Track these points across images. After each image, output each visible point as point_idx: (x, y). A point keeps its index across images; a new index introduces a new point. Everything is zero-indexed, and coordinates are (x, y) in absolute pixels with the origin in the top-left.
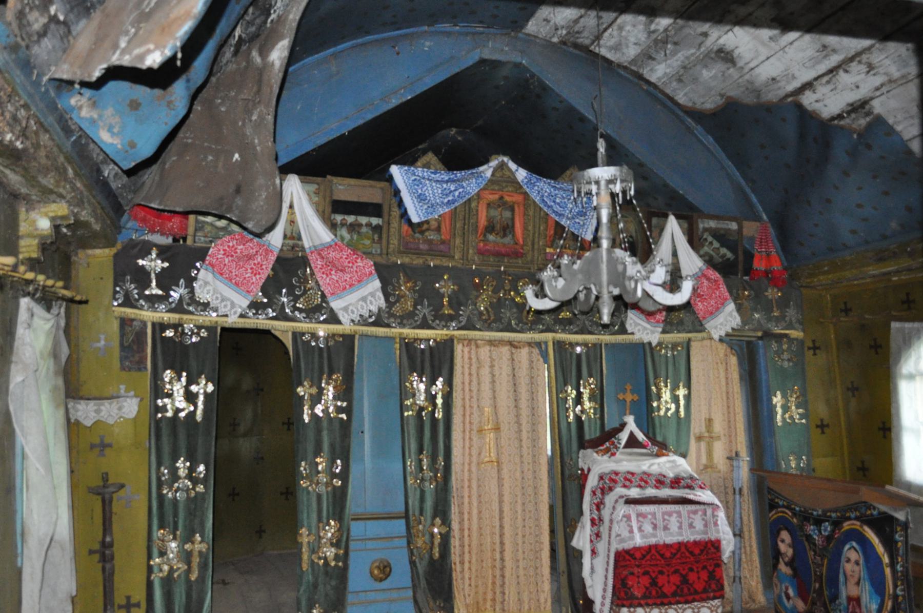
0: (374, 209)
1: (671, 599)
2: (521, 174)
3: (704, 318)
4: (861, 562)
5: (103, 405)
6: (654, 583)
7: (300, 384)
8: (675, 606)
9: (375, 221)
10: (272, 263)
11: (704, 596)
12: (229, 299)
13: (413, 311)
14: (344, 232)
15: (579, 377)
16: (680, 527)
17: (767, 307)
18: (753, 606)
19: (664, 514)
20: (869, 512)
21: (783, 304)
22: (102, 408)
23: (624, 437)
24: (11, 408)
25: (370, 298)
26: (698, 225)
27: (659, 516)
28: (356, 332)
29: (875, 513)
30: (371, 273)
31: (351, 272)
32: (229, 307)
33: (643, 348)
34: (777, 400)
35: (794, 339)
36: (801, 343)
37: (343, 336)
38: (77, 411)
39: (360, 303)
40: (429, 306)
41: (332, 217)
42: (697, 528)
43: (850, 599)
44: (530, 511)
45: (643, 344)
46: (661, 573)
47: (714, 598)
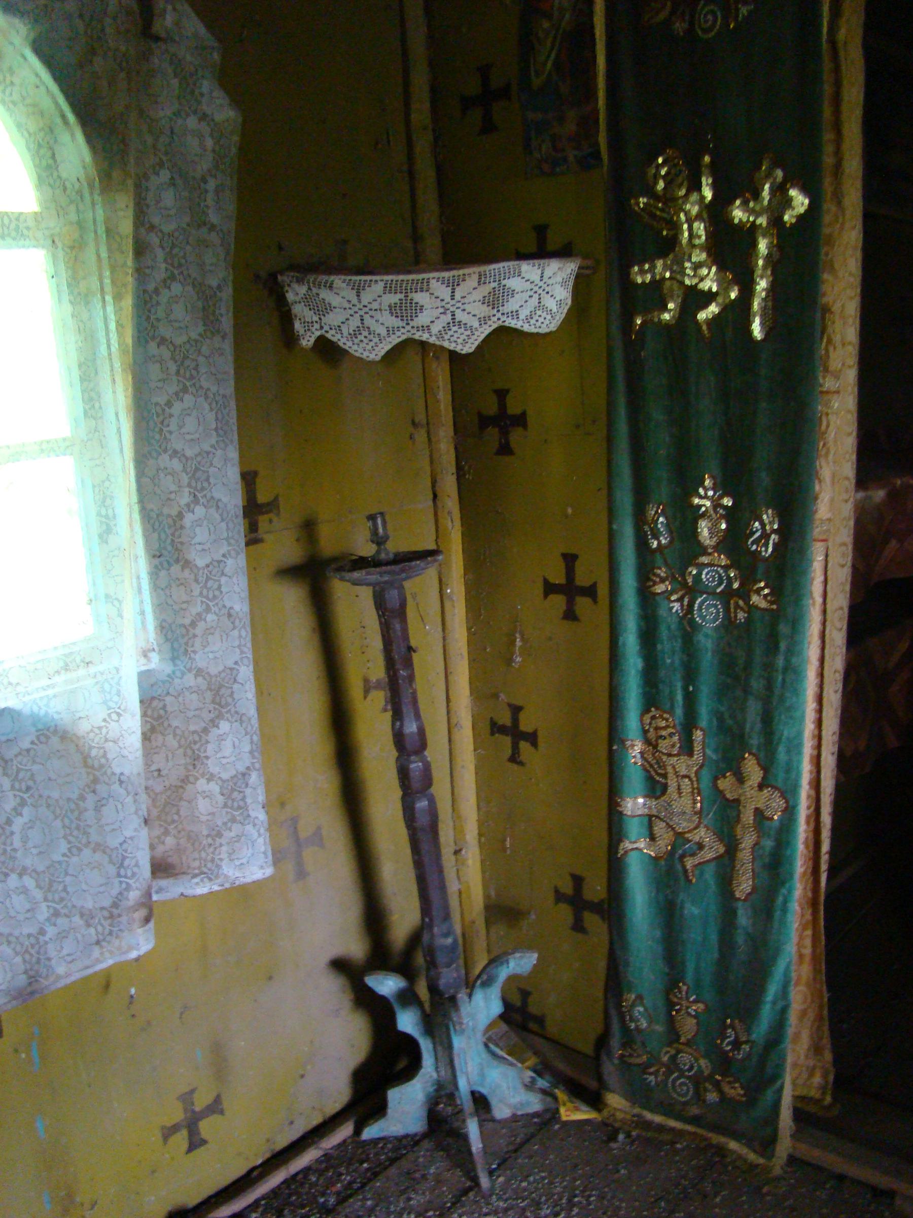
5: (424, 287)
22: (420, 298)
24: (260, 1161)
38: (324, 309)
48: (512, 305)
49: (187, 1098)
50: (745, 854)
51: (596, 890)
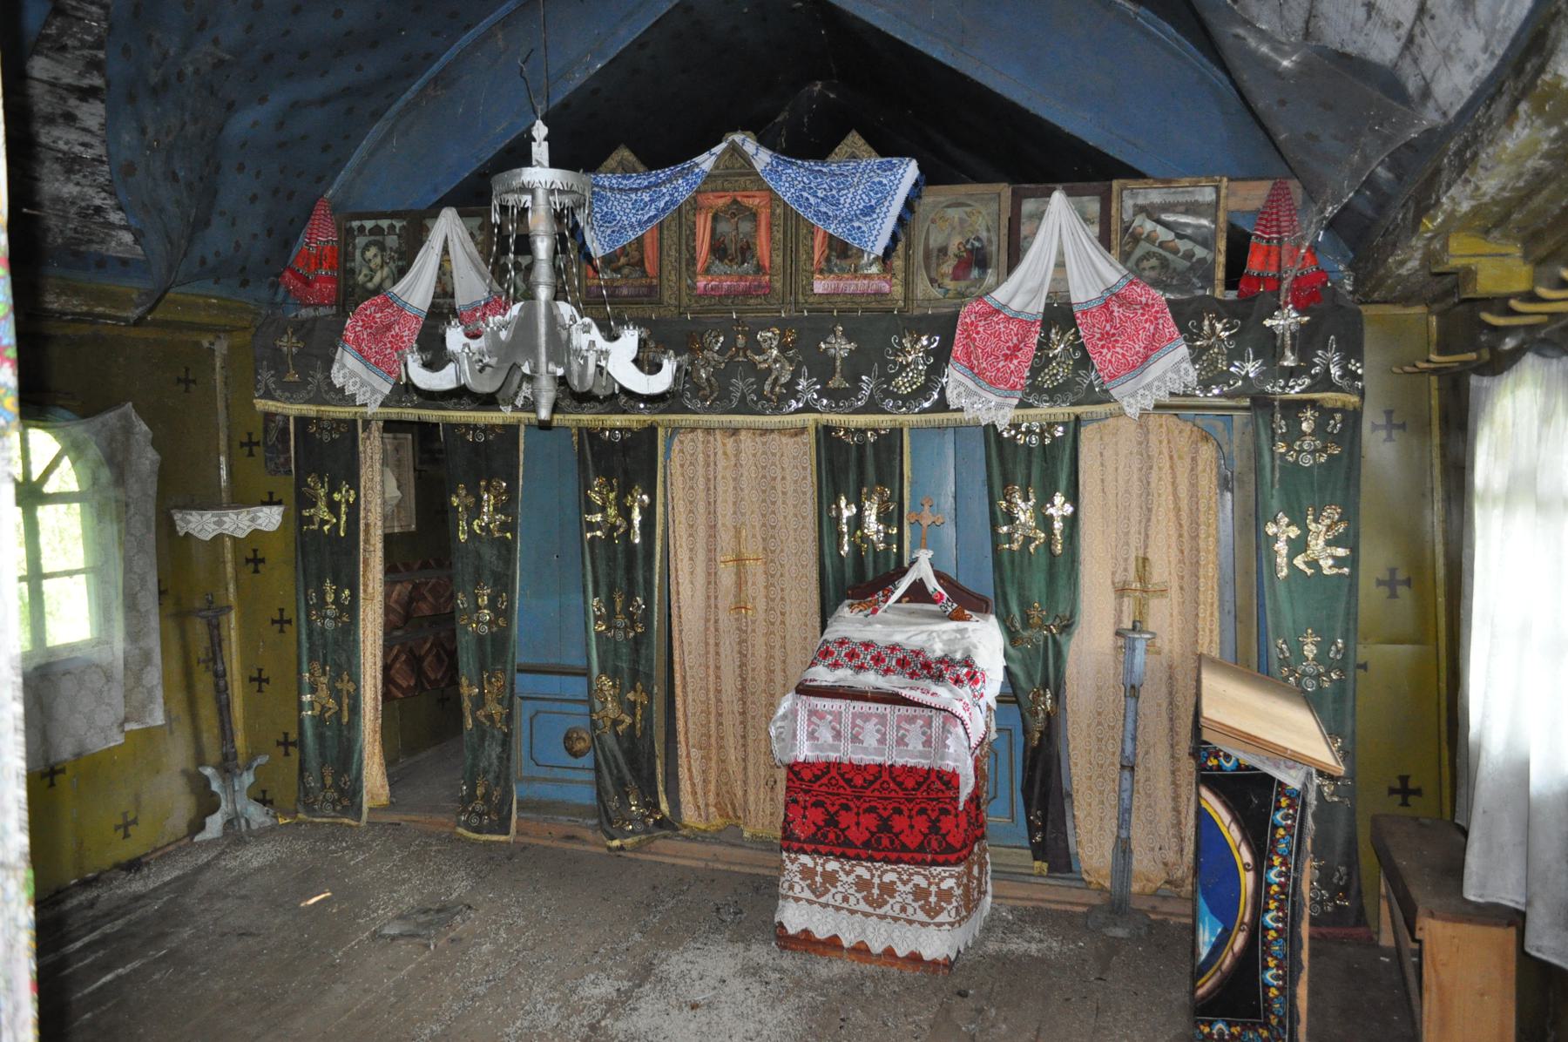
1: (861, 852)
2: (762, 158)
3: (1112, 377)
6: (832, 821)
11: (918, 856)
15: (861, 483)
16: (882, 741)
17: (1268, 347)
23: (904, 585)
27: (847, 719)
29: (1228, 765)
37: (504, 426)
38: (189, 522)
47: (934, 863)
49: (125, 815)
50: (345, 707)
51: (293, 736)
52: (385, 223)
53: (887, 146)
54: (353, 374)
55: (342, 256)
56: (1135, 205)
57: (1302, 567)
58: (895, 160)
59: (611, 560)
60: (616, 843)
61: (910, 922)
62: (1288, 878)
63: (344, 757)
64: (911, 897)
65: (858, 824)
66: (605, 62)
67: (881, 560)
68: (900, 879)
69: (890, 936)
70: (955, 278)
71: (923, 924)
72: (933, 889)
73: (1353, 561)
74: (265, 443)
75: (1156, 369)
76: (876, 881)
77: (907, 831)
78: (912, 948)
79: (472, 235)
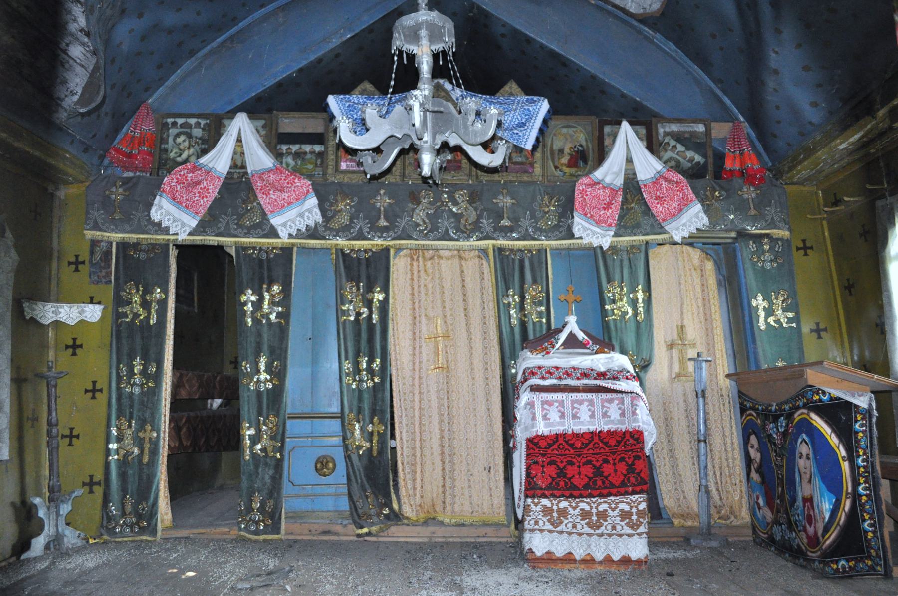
0: (318, 138)
1: (583, 492)
3: (664, 220)
4: (811, 456)
5: (62, 307)
6: (562, 473)
7: (243, 292)
8: (588, 500)
9: (318, 148)
10: (219, 187)
11: (622, 490)
12: (179, 220)
13: (350, 225)
14: (290, 160)
16: (592, 416)
17: (742, 208)
18: (736, 523)
19: (573, 402)
20: (816, 397)
21: (761, 203)
23: (563, 337)
25: (307, 214)
26: (657, 129)
27: (567, 404)
28: (293, 244)
29: (825, 398)
30: (308, 191)
31: (289, 192)
32: (179, 227)
33: (595, 252)
34: (759, 302)
35: (778, 239)
36: (787, 243)
39: (298, 219)
40: (365, 219)
41: (278, 147)
42: (612, 418)
43: (805, 500)
44: (482, 417)
45: (594, 249)
46: (571, 463)
47: (634, 493)
48: (85, 315)
51: (99, 476)
52: (192, 121)
53: (530, 89)
54: (168, 214)
55: (158, 140)
56: (664, 132)
57: (773, 323)
58: (535, 98)
59: (357, 340)
60: (365, 530)
61: (620, 535)
62: (868, 463)
63: (144, 490)
64: (618, 519)
65: (579, 474)
66: (353, 34)
67: (538, 328)
68: (610, 508)
69: (607, 547)
70: (569, 165)
71: (629, 535)
72: (634, 510)
73: (797, 319)
74: (91, 262)
75: (685, 218)
76: (594, 511)
77: (613, 474)
78: (623, 553)
79: (258, 131)
